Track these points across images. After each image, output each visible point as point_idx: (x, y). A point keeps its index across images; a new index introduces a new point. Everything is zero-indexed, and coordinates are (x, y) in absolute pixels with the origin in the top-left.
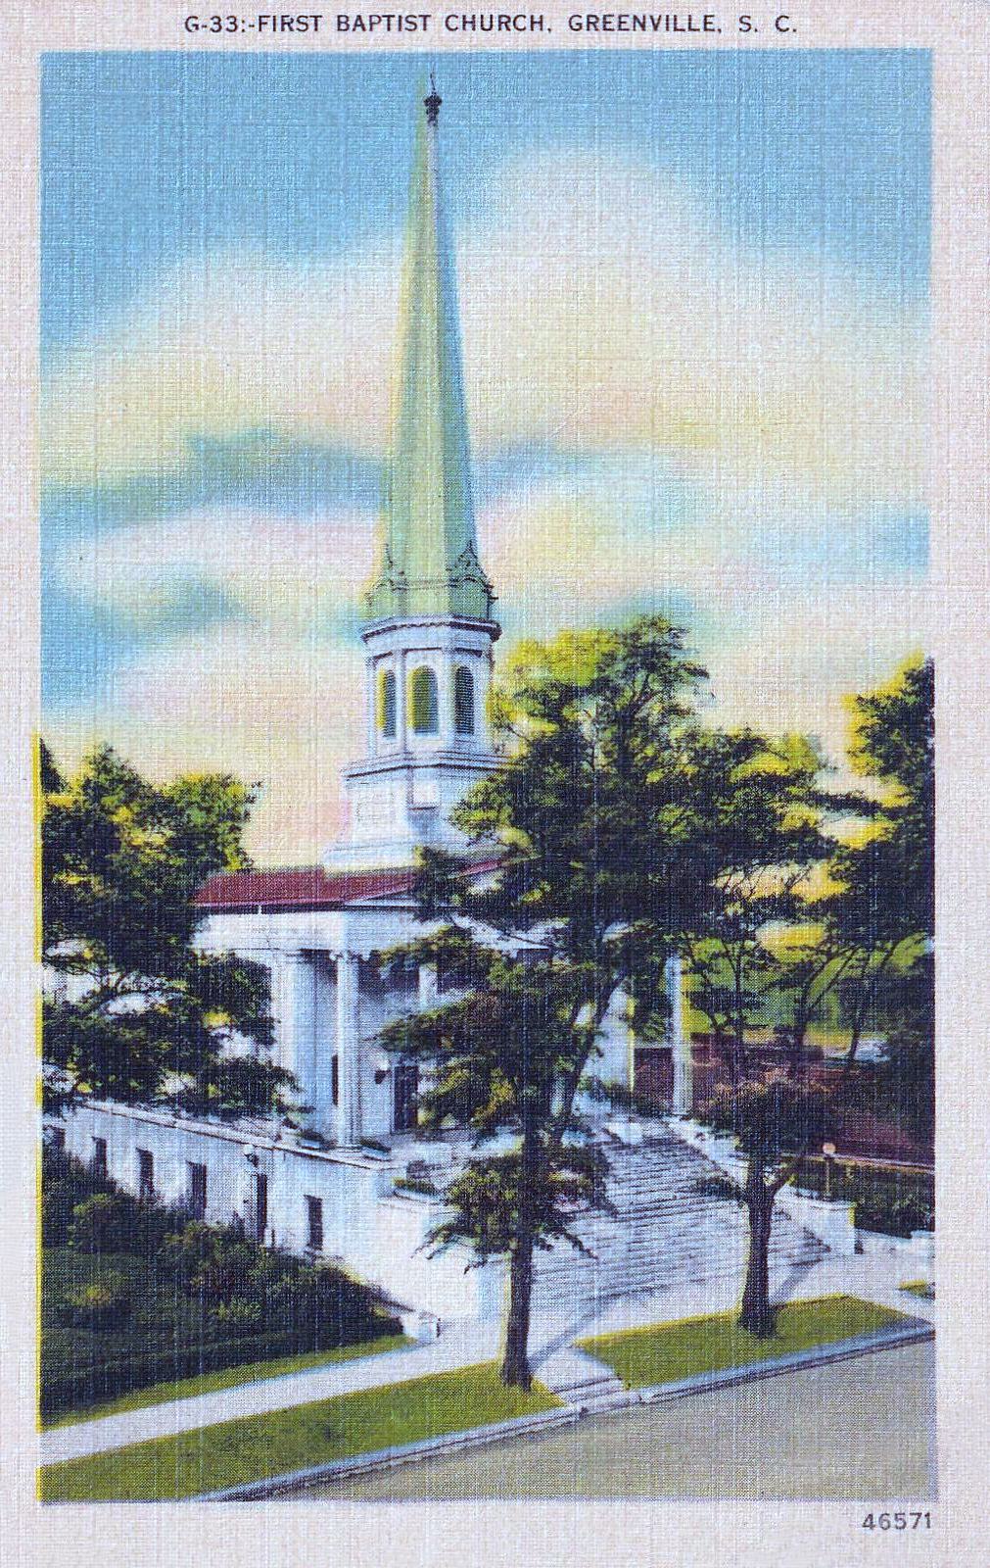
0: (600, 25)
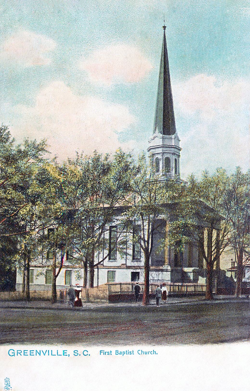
0: (22, 354)
